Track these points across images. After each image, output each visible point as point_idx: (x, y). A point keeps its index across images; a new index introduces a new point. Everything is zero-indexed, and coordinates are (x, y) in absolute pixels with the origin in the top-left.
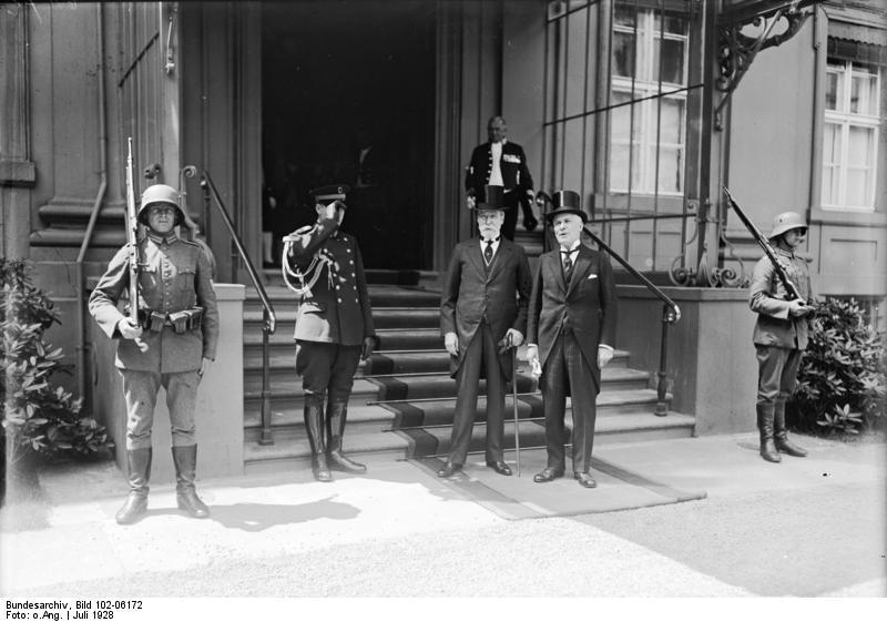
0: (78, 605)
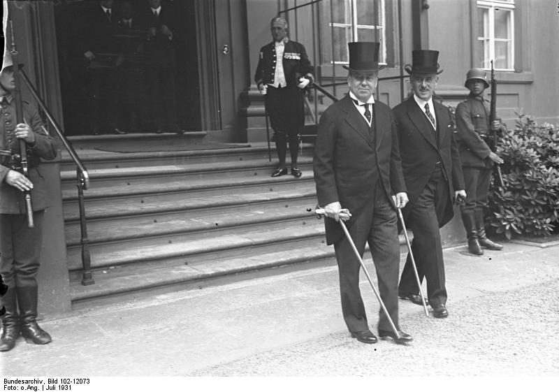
0: (49, 381)
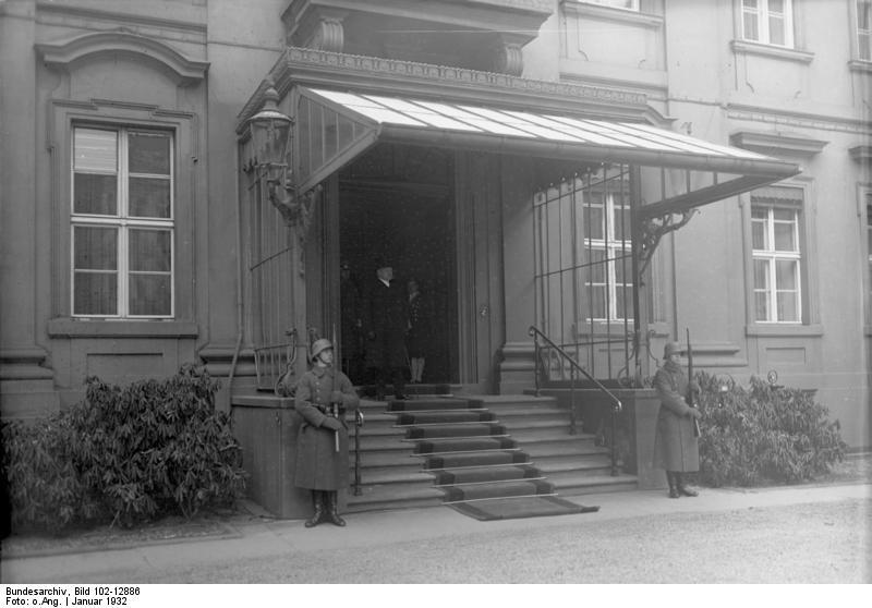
0: (77, 591)
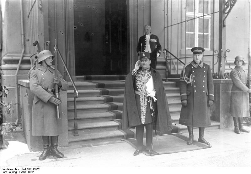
0: (22, 169)
